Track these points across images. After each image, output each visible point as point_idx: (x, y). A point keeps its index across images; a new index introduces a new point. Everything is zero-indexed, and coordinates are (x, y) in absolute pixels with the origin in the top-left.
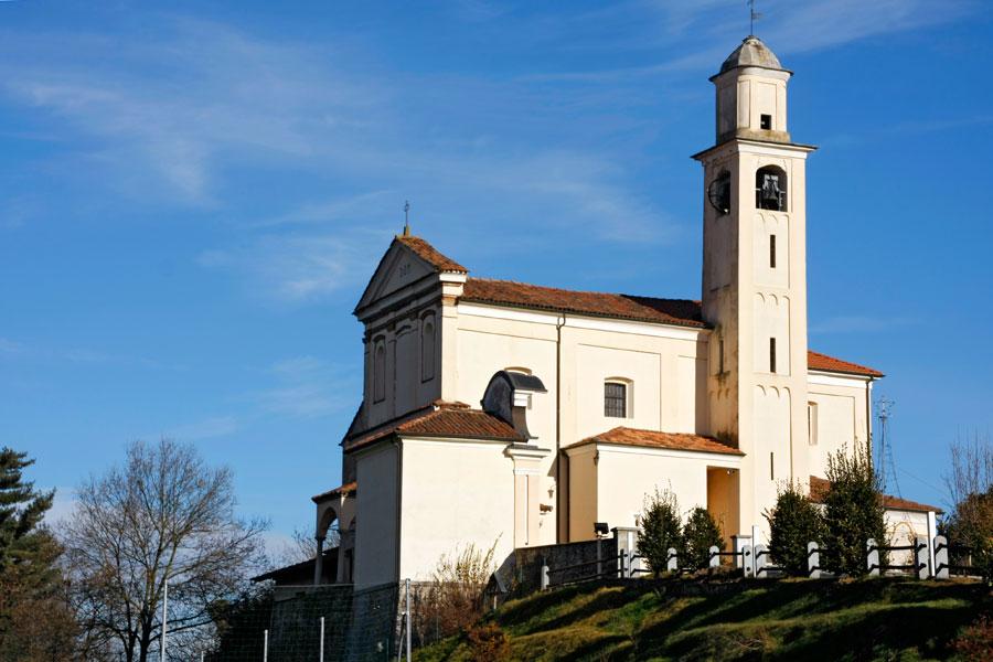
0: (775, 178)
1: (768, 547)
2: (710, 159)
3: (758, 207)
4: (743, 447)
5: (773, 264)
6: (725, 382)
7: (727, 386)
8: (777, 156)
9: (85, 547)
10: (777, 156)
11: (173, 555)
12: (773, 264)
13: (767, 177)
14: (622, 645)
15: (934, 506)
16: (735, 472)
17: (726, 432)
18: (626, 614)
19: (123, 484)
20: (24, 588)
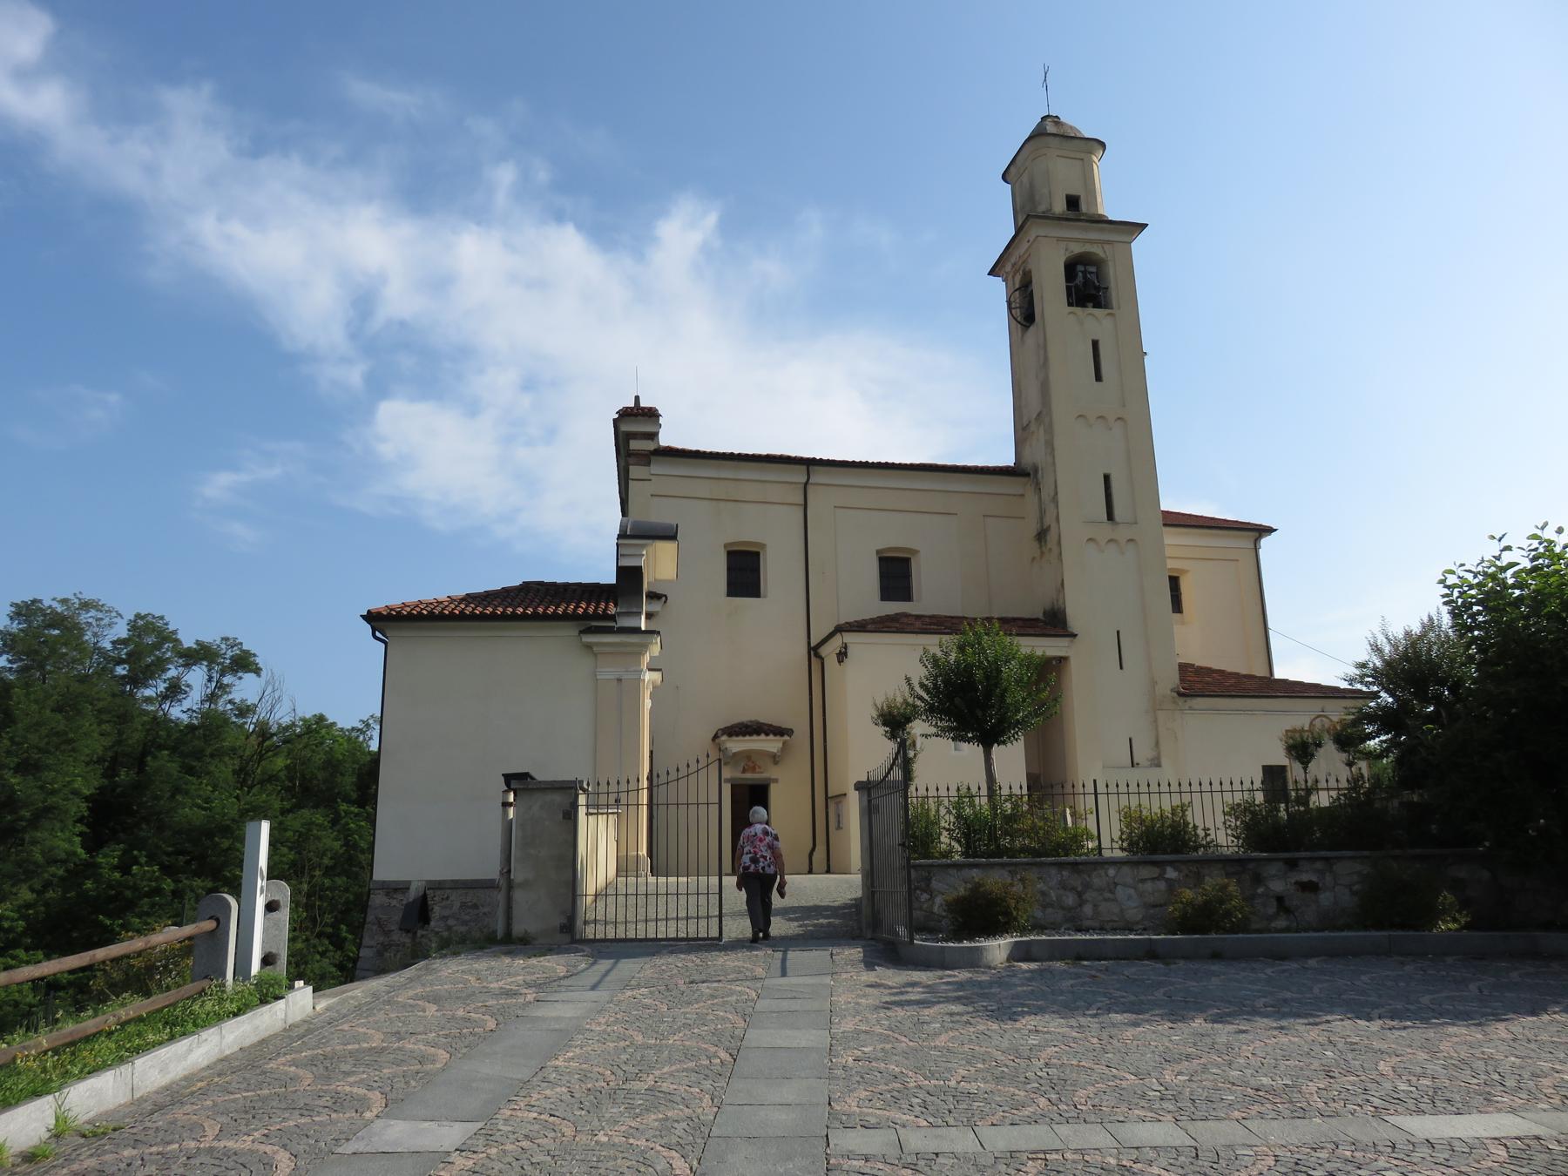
0: (1093, 269)
1: (1395, 646)
2: (1008, 268)
3: (1070, 304)
4: (1074, 623)
5: (1098, 378)
6: (1046, 541)
7: (1049, 546)
8: (1091, 242)
9: (154, 884)
10: (1091, 242)
11: (911, 909)
12: (1098, 378)
13: (1080, 268)
14: (1418, 851)
15: (772, 815)
16: (1062, 660)
17: (1053, 609)
18: (435, 999)
19: (287, 757)
20: (350, 821)
